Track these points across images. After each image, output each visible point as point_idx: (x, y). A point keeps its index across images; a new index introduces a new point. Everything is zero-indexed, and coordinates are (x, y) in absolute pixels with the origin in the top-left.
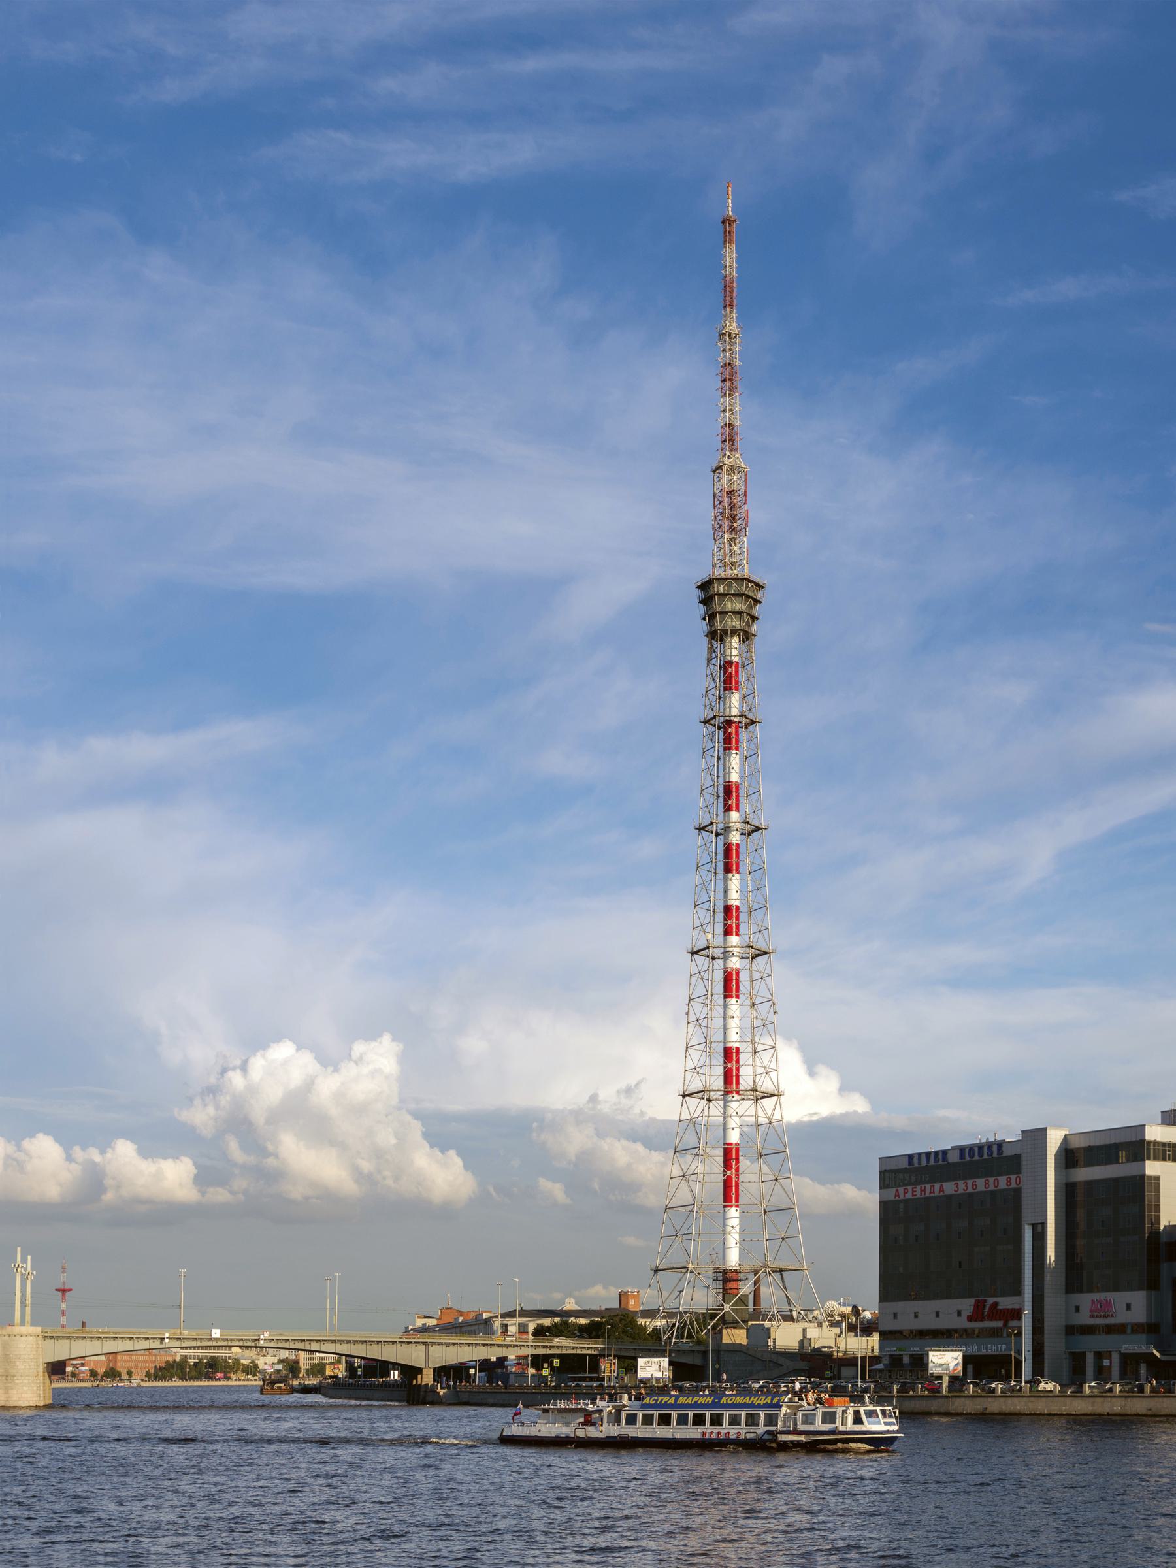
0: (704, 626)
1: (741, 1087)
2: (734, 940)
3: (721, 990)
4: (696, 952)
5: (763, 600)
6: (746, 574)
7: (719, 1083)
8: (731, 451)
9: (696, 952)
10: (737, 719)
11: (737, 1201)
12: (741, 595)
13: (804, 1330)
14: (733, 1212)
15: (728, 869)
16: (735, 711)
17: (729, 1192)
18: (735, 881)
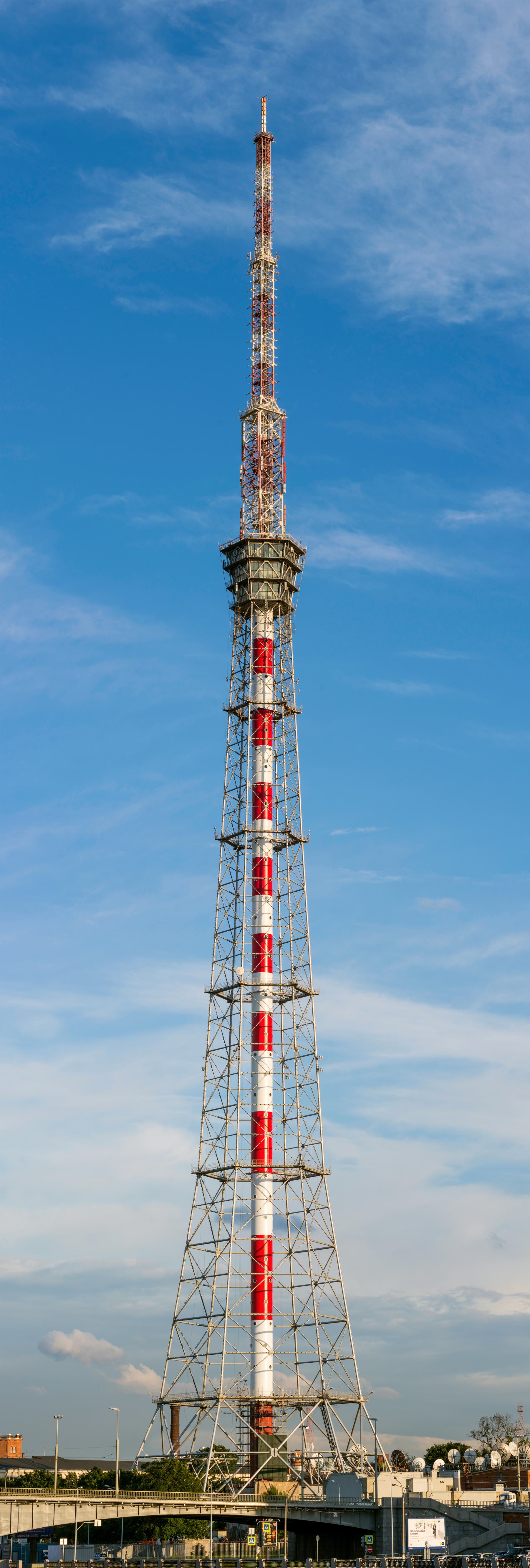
0: (230, 598)
1: (275, 1162)
2: (266, 977)
3: (249, 1040)
4: (205, 1174)
5: (302, 568)
6: (283, 536)
7: (245, 1157)
8: (265, 394)
9: (205, 1174)
10: (270, 708)
11: (270, 1311)
12: (280, 561)
13: (409, 1481)
14: (265, 1325)
15: (258, 888)
16: (269, 698)
17: (259, 1302)
18: (267, 905)
